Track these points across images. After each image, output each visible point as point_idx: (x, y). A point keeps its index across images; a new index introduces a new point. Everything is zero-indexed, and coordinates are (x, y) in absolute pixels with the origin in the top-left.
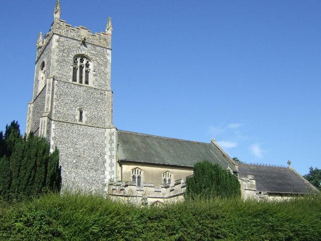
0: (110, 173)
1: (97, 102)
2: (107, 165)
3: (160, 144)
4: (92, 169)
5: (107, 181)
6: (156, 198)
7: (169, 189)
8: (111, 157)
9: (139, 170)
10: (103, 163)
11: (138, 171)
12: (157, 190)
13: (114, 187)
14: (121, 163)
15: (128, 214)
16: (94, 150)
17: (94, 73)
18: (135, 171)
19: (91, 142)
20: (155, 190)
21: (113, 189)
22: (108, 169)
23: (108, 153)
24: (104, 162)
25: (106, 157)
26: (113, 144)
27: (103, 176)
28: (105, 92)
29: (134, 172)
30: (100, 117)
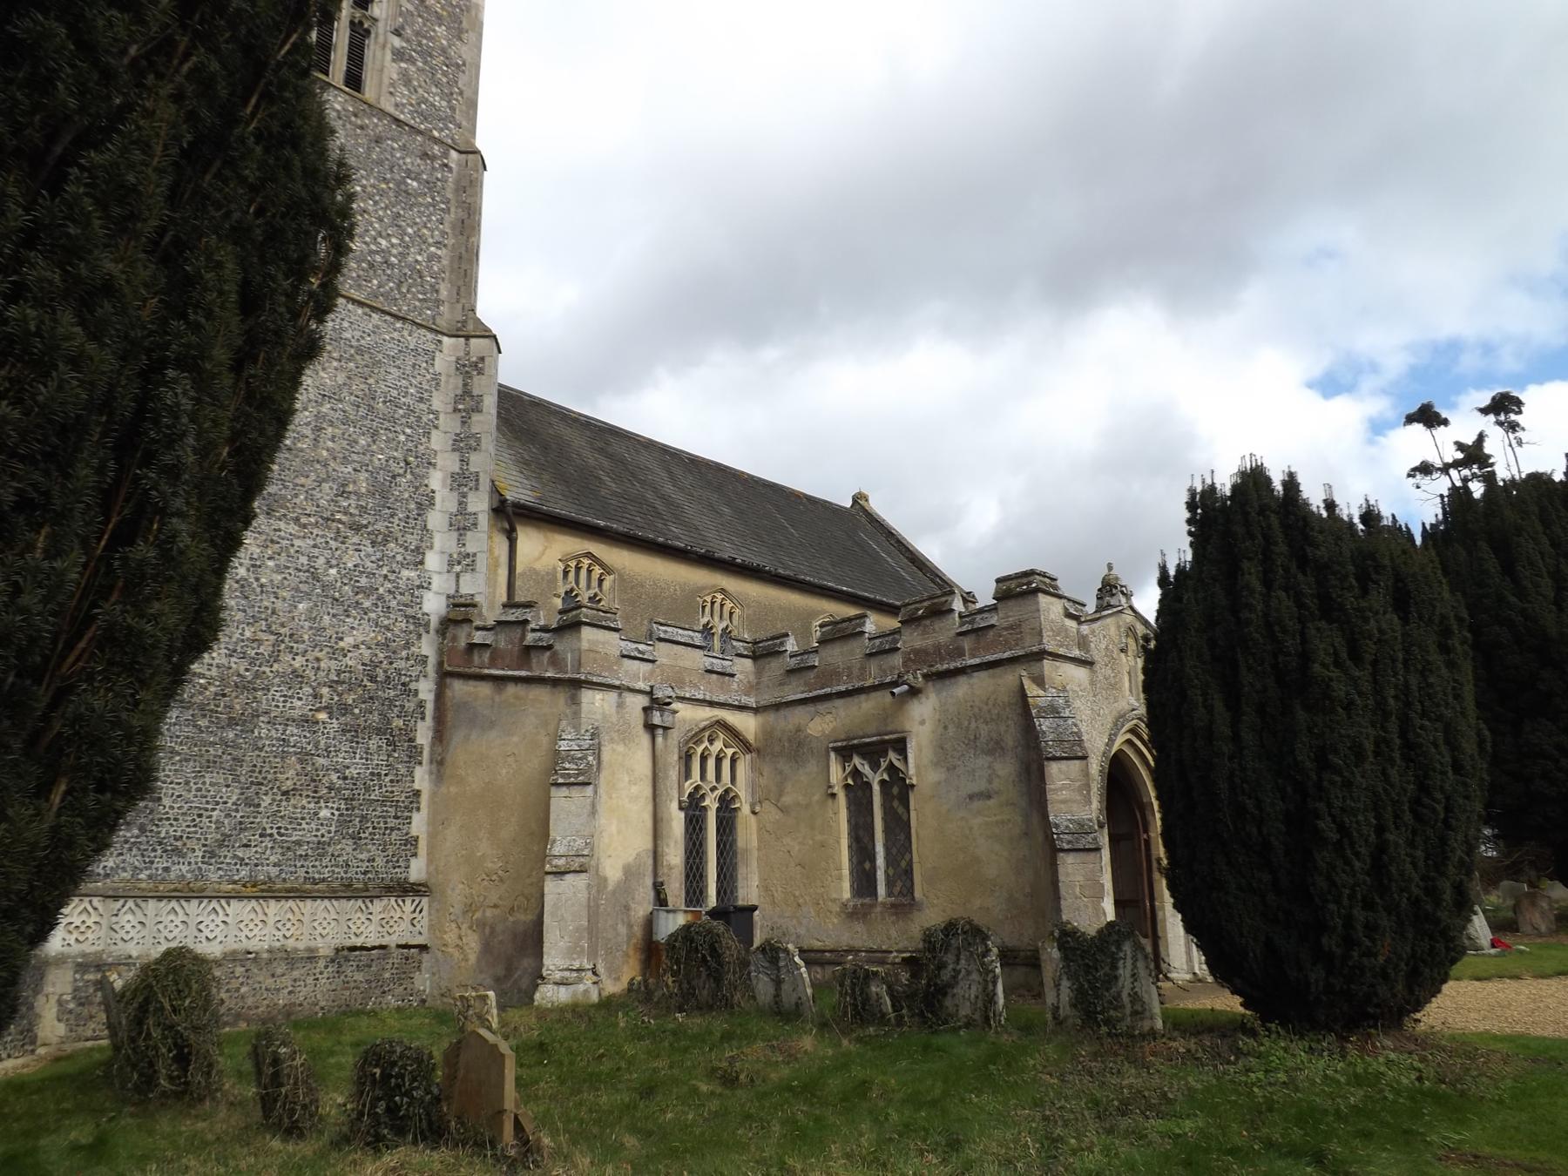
0: (451, 564)
1: (402, 191)
2: (436, 519)
3: (670, 473)
4: (357, 528)
5: (434, 605)
6: (711, 704)
7: (775, 667)
8: (462, 481)
9: (597, 571)
10: (420, 505)
11: (590, 571)
12: (718, 665)
13: (478, 637)
14: (509, 516)
15: (1321, 532)
16: (374, 435)
17: (397, 42)
18: (578, 569)
19: (358, 386)
20: (708, 662)
21: (472, 647)
22: (442, 543)
23: (448, 462)
24: (426, 502)
25: (436, 480)
26: (476, 417)
27: (413, 574)
28: (446, 155)
29: (572, 575)
30: (413, 269)
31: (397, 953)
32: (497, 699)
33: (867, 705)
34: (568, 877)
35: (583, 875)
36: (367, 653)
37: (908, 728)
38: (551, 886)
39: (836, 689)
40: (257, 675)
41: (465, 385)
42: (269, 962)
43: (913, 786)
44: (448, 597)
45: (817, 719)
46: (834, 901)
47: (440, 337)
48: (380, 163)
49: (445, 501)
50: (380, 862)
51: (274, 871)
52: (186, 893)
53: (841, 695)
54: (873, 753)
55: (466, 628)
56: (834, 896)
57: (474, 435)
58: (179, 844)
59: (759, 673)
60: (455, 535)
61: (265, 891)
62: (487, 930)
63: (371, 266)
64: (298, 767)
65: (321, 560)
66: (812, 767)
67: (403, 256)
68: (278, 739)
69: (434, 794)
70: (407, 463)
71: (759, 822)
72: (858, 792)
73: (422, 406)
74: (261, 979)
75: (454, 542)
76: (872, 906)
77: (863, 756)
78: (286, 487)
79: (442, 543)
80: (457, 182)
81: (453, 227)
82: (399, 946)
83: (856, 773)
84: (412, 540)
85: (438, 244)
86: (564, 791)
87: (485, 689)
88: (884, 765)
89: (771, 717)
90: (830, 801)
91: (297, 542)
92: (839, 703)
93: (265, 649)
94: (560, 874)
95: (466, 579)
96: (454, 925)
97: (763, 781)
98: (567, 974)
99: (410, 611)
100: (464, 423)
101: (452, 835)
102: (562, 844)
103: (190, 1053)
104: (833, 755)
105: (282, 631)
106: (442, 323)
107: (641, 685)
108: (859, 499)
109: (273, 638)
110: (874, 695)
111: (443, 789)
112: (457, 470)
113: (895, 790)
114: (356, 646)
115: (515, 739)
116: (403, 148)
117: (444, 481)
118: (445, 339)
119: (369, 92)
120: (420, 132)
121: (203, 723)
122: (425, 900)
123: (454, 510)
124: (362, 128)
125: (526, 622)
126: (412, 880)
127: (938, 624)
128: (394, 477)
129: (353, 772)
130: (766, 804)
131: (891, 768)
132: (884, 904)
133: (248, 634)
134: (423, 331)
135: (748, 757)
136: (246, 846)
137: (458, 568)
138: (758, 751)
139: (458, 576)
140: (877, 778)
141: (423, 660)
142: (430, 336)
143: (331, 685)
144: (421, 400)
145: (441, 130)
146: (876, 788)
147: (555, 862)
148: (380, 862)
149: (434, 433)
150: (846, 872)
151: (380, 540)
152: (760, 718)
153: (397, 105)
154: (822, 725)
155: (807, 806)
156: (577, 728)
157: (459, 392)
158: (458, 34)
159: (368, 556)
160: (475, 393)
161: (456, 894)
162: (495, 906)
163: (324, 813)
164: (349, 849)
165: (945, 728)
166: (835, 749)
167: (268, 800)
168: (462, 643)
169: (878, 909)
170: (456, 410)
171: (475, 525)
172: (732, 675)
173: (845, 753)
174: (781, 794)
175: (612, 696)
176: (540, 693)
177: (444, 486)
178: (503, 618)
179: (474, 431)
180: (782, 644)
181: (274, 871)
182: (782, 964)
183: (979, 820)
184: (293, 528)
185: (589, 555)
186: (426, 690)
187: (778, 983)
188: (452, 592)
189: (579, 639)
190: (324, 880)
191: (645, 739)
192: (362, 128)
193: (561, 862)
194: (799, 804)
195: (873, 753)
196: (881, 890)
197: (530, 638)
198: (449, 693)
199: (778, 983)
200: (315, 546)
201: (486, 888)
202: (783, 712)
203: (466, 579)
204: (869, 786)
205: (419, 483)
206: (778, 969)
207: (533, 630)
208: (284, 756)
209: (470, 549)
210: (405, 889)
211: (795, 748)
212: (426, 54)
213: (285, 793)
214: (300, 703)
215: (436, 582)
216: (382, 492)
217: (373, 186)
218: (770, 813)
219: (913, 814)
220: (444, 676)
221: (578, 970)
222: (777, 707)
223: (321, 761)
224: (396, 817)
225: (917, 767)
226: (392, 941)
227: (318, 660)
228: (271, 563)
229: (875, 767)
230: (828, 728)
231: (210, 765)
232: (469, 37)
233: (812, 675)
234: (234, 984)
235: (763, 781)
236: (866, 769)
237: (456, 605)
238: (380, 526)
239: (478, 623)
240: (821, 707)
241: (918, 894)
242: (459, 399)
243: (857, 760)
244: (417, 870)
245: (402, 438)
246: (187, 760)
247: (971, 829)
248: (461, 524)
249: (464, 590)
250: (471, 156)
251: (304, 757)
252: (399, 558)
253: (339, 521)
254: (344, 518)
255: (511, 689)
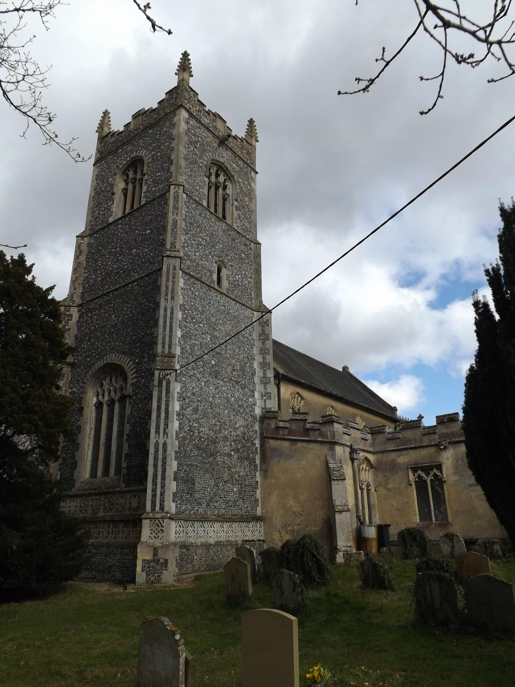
2: (257, 379)
4: (237, 383)
5: (258, 411)
7: (381, 438)
8: (264, 365)
13: (281, 424)
14: (279, 378)
17: (236, 203)
22: (259, 388)
25: (256, 365)
26: (267, 342)
31: (257, 543)
32: (293, 447)
33: (424, 452)
34: (343, 513)
35: (349, 512)
36: (242, 429)
37: (441, 460)
38: (338, 516)
39: (410, 446)
40: (216, 437)
41: (263, 330)
42: (227, 545)
43: (445, 481)
44: (262, 408)
45: (401, 457)
46: (414, 523)
47: (253, 312)
48: (234, 248)
49: (259, 373)
50: (249, 508)
51: (224, 511)
52: (204, 519)
53: (412, 448)
54: (427, 470)
55: (274, 420)
56: (413, 521)
57: (267, 349)
58: (200, 501)
59: (374, 439)
60: (263, 385)
61: (222, 519)
62: (295, 534)
63: (235, 285)
64: (228, 472)
65: (230, 395)
66: (400, 474)
67: (242, 281)
68: (222, 462)
69: (262, 484)
70: (248, 359)
71: (377, 494)
72: (421, 485)
73: (251, 337)
74: (224, 552)
75: (263, 388)
76: (430, 525)
77: (422, 471)
78: (220, 368)
79: (259, 388)
80: (254, 254)
81: (254, 271)
82: (259, 540)
83: (420, 477)
84: (251, 387)
85: (250, 277)
86: (336, 482)
87: (286, 444)
88: (432, 474)
89: (380, 456)
90: (409, 487)
91: (223, 388)
92: (410, 451)
93: (218, 428)
94: (341, 512)
95: (268, 402)
96: (277, 532)
97: (379, 479)
98: (346, 548)
99: (252, 414)
100: (263, 344)
101: (274, 499)
102: (338, 501)
103: (323, 569)
104: (410, 470)
105: (222, 421)
106: (253, 307)
107: (348, 444)
108: (345, 368)
109: (219, 423)
110: (426, 449)
111: (268, 481)
112: (262, 361)
113: (437, 483)
114: (240, 427)
115: (303, 463)
116: (240, 242)
117: (258, 365)
118: (255, 313)
119: (229, 220)
120: (244, 236)
121: (204, 455)
122: (262, 523)
123: (262, 376)
124: (230, 235)
125: (306, 420)
126: (258, 515)
127: (452, 424)
128: (245, 364)
129: (241, 474)
130: (380, 488)
131: (435, 475)
132: (435, 524)
133: (213, 422)
134: (249, 310)
135: (372, 470)
136: (217, 502)
137: (265, 398)
138: (376, 468)
139: (265, 401)
140: (429, 479)
141: (256, 432)
142: (251, 311)
143: (235, 441)
144: (250, 335)
145: (248, 235)
146: (429, 482)
147: (338, 507)
148: (249, 508)
149: (254, 347)
150: (417, 512)
151: (243, 387)
152: (375, 456)
153: (237, 227)
154: (403, 459)
155: (399, 488)
156: (334, 459)
157: (261, 332)
158: (251, 200)
159: (241, 393)
160: (266, 333)
161: (278, 520)
162: (298, 525)
163: (235, 489)
164: (242, 503)
165: (458, 461)
166: (411, 468)
167: (221, 484)
168: (273, 426)
169: (433, 526)
170: (260, 339)
171: (270, 382)
172: (367, 440)
173: (415, 470)
174: (387, 484)
175: (342, 447)
176: (312, 446)
177: (258, 367)
178: (294, 418)
179: (267, 347)
180: (384, 429)
181: (224, 511)
182: (455, 540)
183: (474, 493)
184: (222, 383)
185: (298, 393)
186: (257, 442)
187: (453, 547)
188: (263, 407)
189: (333, 427)
190: (236, 515)
191: (350, 463)
192: (230, 235)
193: (340, 507)
194: (395, 488)
195: (427, 470)
196: (434, 519)
197: (308, 426)
198: (267, 445)
199: (453, 547)
200: (228, 390)
201: (293, 518)
202: (385, 454)
203: (268, 402)
204: (426, 482)
205: (251, 367)
206: (453, 542)
207: (309, 423)
208: (224, 468)
209: (269, 390)
210: (257, 519)
211: (393, 467)
212: (243, 207)
213: (225, 482)
214: (227, 448)
215: (258, 403)
216: (243, 369)
217: (234, 256)
218: (383, 491)
219: (446, 492)
220: (263, 439)
221: (350, 547)
222: (383, 452)
223: (233, 470)
224: (253, 491)
225: (446, 475)
226: (255, 538)
227: (231, 432)
228: (217, 396)
229: (428, 474)
230: (406, 461)
231: (206, 471)
232: (253, 200)
233: (398, 441)
234: (218, 554)
235: (379, 479)
236: (424, 475)
237: (266, 412)
238: (243, 382)
239: (279, 419)
240: (403, 453)
241: (450, 520)
242: (260, 335)
243: (420, 472)
244: (259, 512)
245: (246, 349)
246: (201, 469)
247: (471, 497)
248: (265, 382)
249: (268, 406)
250: (258, 245)
251: (229, 468)
252: (248, 394)
253: (233, 380)
254: (234, 379)
255: (300, 444)
